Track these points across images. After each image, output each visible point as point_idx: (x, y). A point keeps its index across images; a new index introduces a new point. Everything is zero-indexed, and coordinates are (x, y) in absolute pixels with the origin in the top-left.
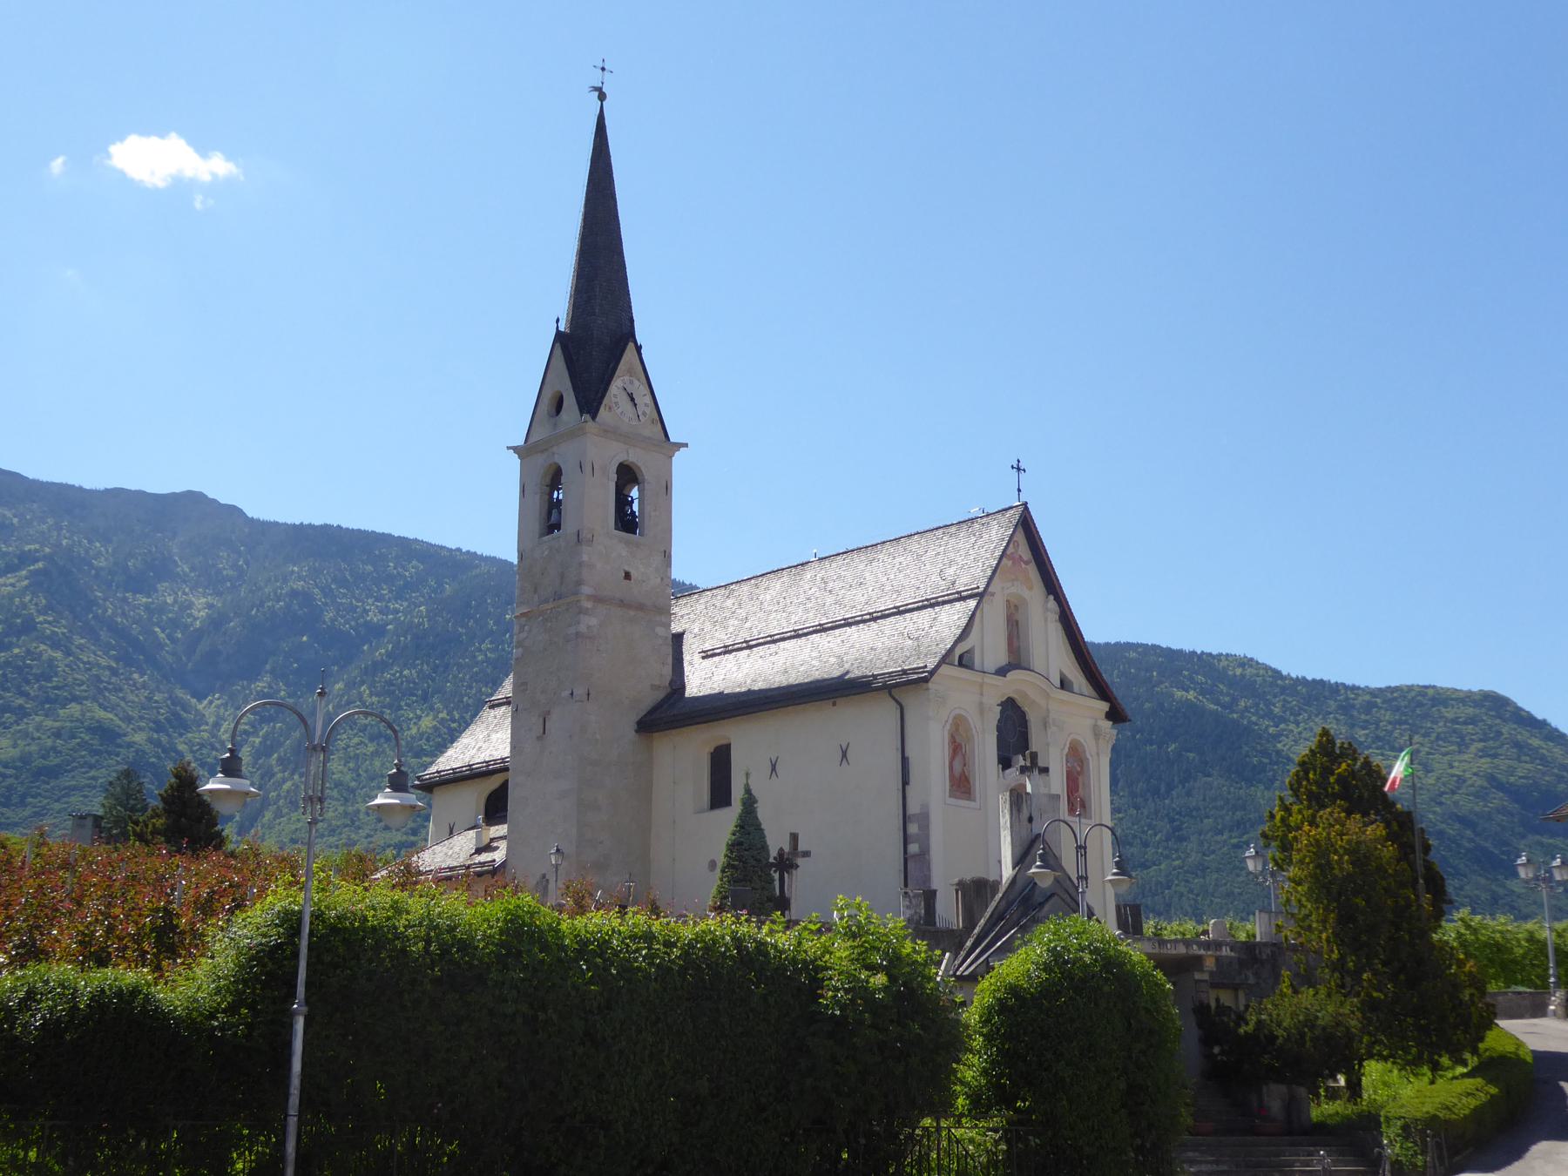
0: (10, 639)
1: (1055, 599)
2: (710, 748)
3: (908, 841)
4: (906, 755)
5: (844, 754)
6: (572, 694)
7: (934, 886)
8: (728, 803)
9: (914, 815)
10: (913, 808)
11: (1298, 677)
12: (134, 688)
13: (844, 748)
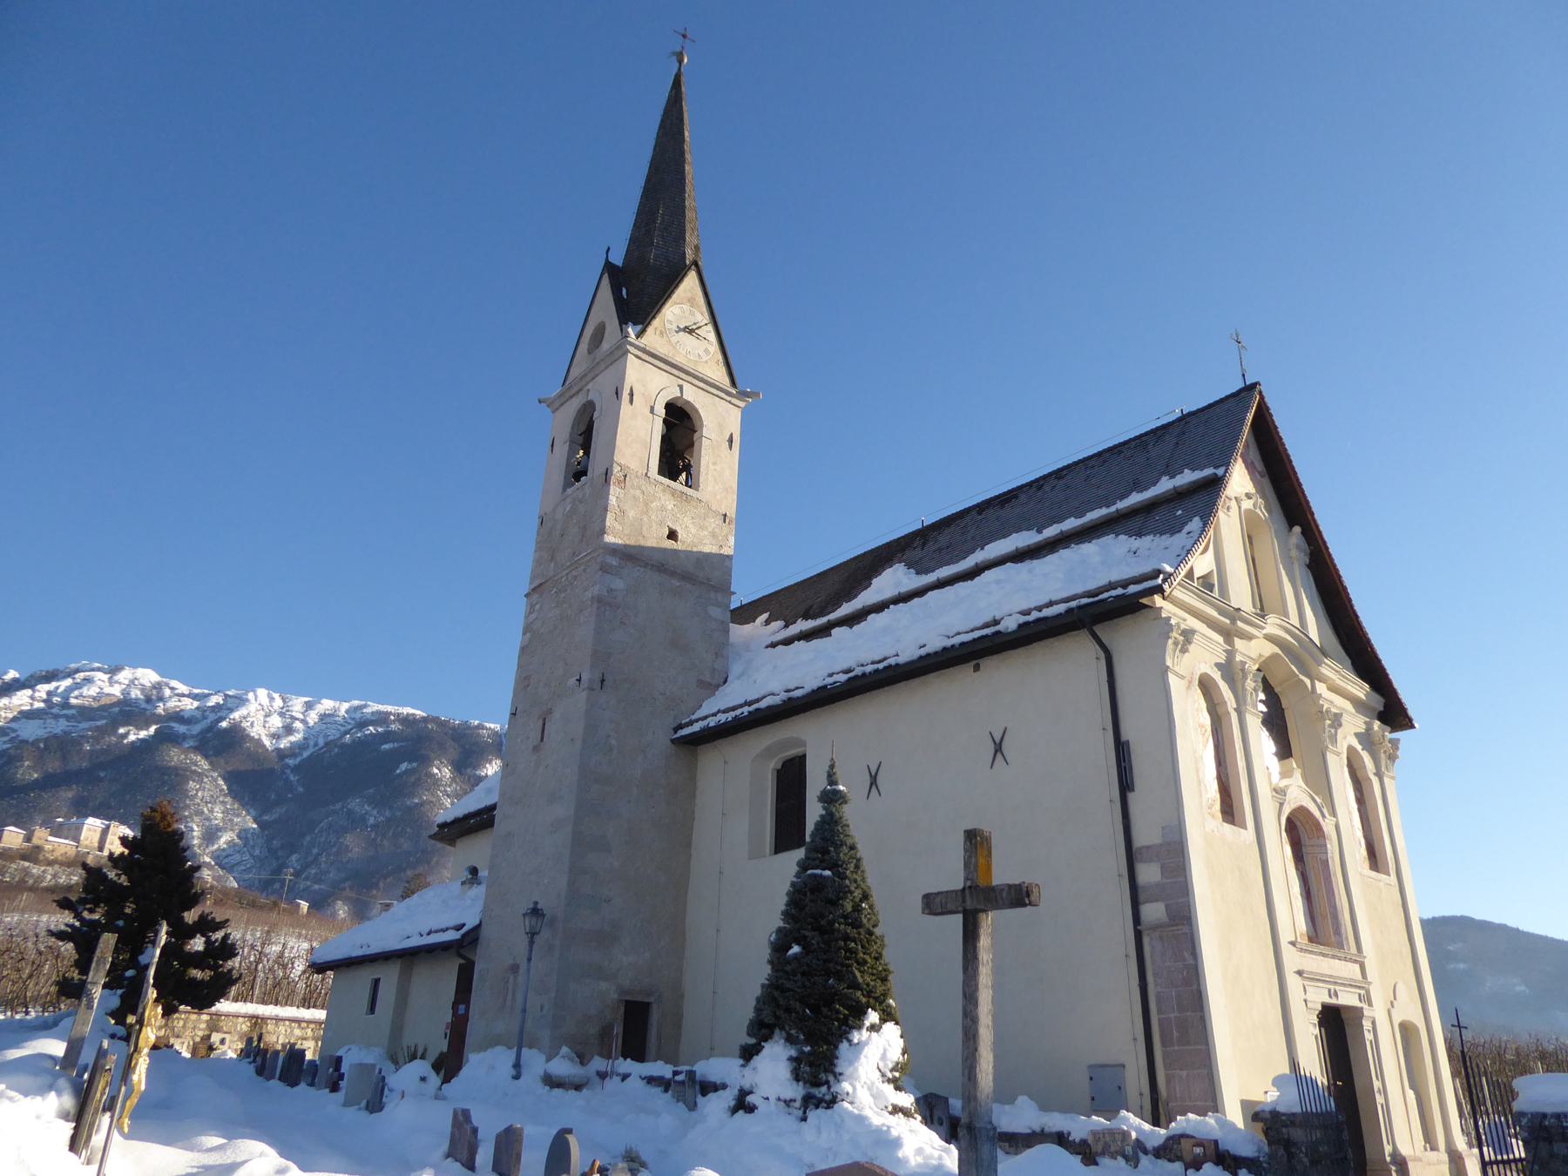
1: (1302, 533)
2: (774, 764)
3: (1142, 897)
4: (1124, 738)
5: (998, 748)
6: (579, 680)
9: (1148, 847)
10: (1144, 836)
11: (625, 1059)
13: (998, 741)
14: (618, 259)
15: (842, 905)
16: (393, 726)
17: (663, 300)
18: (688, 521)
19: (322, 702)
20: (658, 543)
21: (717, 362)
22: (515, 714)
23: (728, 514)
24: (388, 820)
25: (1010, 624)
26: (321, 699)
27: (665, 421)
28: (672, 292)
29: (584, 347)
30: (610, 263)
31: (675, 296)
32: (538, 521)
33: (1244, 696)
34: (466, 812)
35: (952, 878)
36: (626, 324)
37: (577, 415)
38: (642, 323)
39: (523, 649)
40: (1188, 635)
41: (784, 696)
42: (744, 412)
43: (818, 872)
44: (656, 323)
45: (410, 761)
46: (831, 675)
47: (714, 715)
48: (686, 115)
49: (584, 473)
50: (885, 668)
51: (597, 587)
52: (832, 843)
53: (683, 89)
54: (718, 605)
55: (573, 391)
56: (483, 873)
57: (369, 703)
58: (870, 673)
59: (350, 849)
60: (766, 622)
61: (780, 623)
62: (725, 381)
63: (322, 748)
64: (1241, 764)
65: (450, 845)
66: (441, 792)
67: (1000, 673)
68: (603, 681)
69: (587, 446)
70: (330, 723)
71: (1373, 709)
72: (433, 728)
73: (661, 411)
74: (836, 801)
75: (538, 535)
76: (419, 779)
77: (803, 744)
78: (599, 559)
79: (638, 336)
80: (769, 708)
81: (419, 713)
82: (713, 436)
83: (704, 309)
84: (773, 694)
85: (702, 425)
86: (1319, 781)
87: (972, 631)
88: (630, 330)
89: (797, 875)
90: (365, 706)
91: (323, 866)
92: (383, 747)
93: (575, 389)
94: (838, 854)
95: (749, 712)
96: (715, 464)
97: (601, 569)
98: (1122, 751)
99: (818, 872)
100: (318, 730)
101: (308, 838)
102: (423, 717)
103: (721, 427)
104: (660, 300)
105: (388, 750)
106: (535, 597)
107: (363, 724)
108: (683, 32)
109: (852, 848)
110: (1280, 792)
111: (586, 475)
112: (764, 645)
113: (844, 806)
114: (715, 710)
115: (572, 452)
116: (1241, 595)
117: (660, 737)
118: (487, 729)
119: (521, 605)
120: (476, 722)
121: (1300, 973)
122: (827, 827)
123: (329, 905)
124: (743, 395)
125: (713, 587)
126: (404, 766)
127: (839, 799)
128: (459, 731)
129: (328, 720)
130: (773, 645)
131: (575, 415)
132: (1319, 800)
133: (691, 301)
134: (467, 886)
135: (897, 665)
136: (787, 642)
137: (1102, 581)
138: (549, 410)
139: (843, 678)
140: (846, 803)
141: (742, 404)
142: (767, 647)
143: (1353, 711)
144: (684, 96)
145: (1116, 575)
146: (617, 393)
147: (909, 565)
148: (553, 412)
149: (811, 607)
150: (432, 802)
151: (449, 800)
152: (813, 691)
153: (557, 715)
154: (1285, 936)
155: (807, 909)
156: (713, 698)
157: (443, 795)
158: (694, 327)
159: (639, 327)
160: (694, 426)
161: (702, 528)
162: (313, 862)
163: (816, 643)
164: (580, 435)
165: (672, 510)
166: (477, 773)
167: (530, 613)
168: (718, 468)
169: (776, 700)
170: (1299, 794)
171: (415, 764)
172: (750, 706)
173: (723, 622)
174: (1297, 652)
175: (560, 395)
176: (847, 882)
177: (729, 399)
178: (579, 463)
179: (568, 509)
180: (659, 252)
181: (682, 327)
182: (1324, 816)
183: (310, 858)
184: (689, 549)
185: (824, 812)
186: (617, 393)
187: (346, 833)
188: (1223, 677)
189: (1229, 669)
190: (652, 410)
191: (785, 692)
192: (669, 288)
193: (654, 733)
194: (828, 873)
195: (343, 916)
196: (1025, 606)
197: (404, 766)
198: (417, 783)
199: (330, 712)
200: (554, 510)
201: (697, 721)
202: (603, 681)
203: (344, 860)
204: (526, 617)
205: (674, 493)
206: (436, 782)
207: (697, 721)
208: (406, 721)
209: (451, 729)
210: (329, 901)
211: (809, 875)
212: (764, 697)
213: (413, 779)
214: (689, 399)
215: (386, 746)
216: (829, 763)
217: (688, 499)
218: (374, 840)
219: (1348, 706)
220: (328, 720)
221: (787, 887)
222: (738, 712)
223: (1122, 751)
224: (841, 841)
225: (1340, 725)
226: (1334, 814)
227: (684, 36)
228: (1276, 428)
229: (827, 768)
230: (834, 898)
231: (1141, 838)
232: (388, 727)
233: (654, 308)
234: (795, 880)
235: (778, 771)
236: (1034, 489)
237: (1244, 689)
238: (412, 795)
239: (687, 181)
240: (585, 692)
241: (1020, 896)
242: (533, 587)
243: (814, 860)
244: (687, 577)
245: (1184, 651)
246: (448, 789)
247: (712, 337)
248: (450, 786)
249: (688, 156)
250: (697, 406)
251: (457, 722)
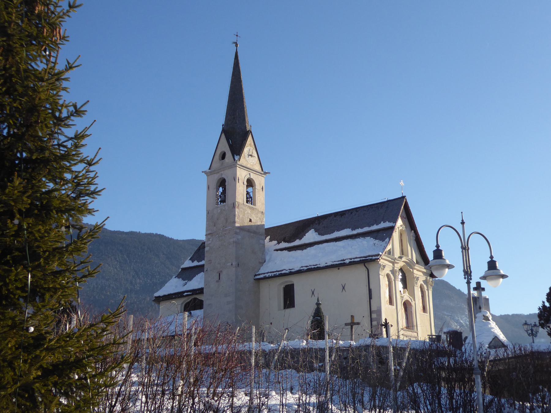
2: (283, 286)
4: (370, 288)
5: (344, 288)
6: (232, 264)
9: (374, 311)
10: (373, 309)
13: (343, 286)
18: (253, 215)
25: (347, 261)
33: (396, 277)
35: (349, 321)
40: (384, 266)
41: (289, 271)
46: (302, 267)
62: (260, 170)
64: (394, 292)
67: (343, 271)
71: (428, 274)
84: (285, 270)
86: (412, 294)
87: (338, 261)
96: (259, 197)
98: (370, 291)
103: (260, 184)
106: (209, 236)
109: (323, 313)
110: (402, 297)
116: (397, 254)
117: (251, 278)
121: (403, 335)
132: (411, 298)
133: (250, 145)
135: (320, 267)
136: (282, 250)
137: (367, 255)
143: (423, 275)
145: (370, 254)
147: (316, 231)
152: (297, 271)
154: (401, 327)
168: (260, 198)
169: (287, 272)
170: (407, 297)
174: (410, 264)
177: (261, 175)
182: (412, 301)
188: (391, 273)
189: (393, 272)
190: (244, 184)
194: (319, 318)
196: (350, 257)
202: (238, 265)
205: (250, 208)
217: (253, 209)
219: (421, 274)
222: (275, 273)
223: (370, 291)
225: (418, 280)
226: (415, 300)
227: (237, 36)
228: (409, 207)
231: (373, 309)
236: (350, 213)
237: (396, 275)
241: (358, 324)
244: (255, 232)
245: (383, 270)
247: (256, 155)
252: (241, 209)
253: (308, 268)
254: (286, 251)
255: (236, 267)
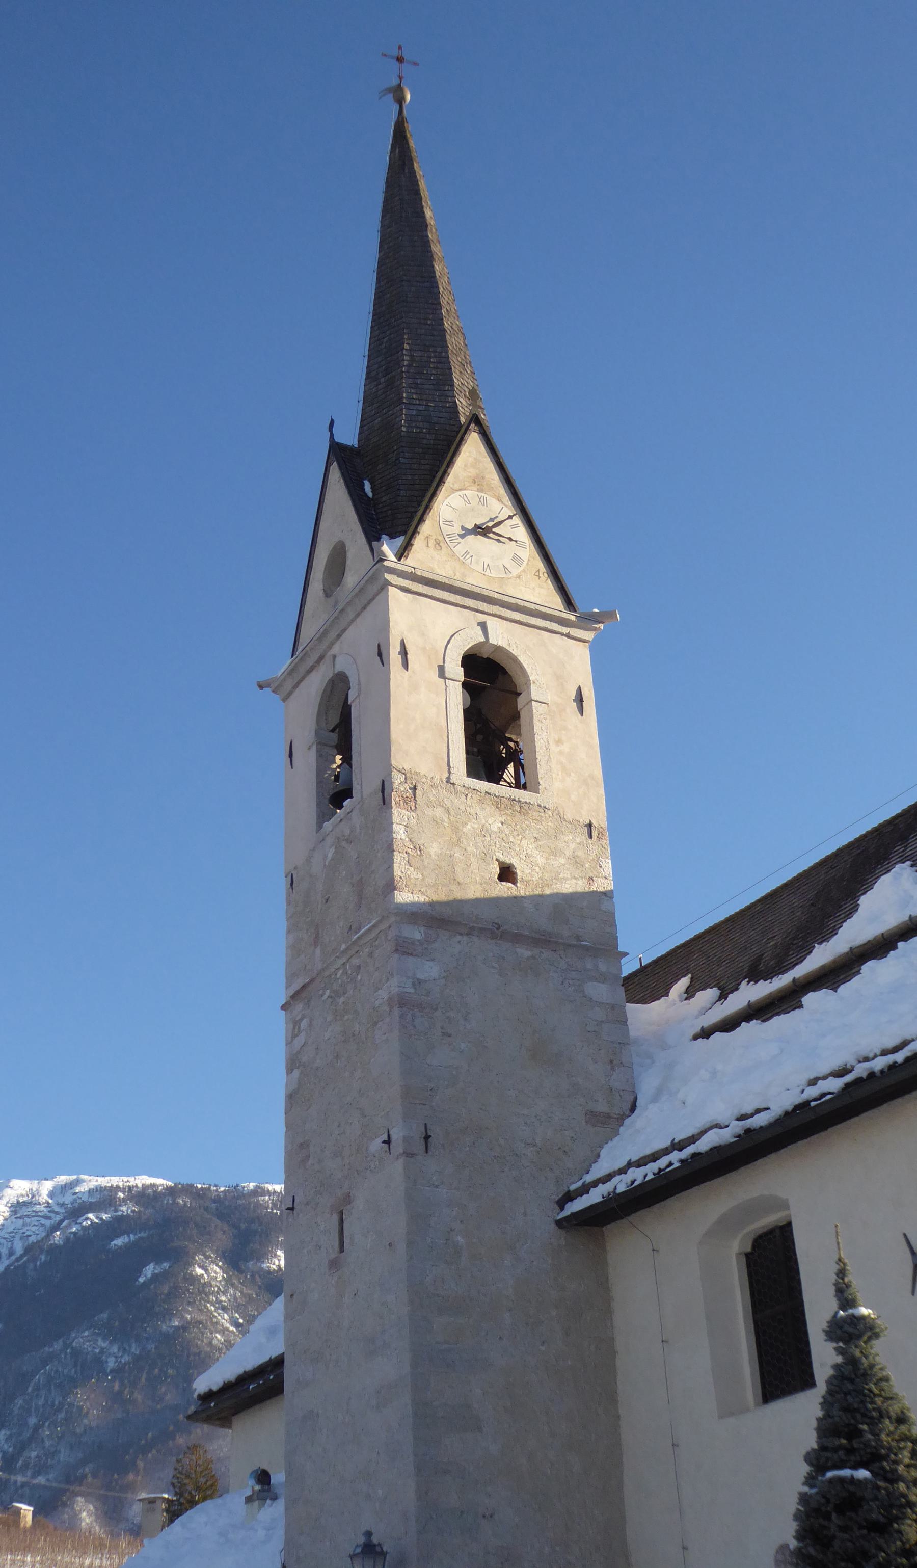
0: (136, 1237)
6: (388, 1142)
7: (285, 878)
8: (808, 1382)
12: (841, 1281)
14: (349, 436)
15: (900, 1532)
16: (124, 1209)
17: (432, 489)
18: (528, 845)
19: (11, 1184)
20: (484, 890)
21: (537, 574)
22: (292, 1209)
23: (594, 822)
24: (137, 1359)
26: (9, 1180)
27: (465, 685)
28: (445, 473)
29: (317, 585)
30: (338, 444)
31: (450, 480)
32: (283, 883)
34: (240, 1371)
36: (378, 539)
37: (322, 699)
38: (404, 533)
39: (292, 1098)
41: (737, 1127)
42: (596, 650)
43: (846, 1473)
44: (426, 528)
45: (158, 1262)
46: (813, 1082)
47: (623, 1171)
48: (422, 184)
49: (347, 793)
50: (908, 1060)
51: (395, 981)
52: (864, 1415)
53: (412, 143)
54: (603, 978)
55: (310, 662)
56: (278, 1478)
57: (82, 1177)
58: (882, 1071)
59: (85, 1410)
60: (686, 992)
61: (711, 993)
62: (551, 600)
63: (22, 1256)
65: (223, 1426)
66: (212, 1304)
68: (427, 1138)
69: (345, 747)
70: (27, 1216)
72: (185, 1204)
73: (457, 671)
74: (859, 1337)
75: (289, 903)
76: (176, 1287)
77: (785, 1205)
78: (392, 934)
79: (401, 554)
80: (716, 1150)
81: (161, 1182)
82: (548, 698)
83: (502, 491)
85: (528, 683)
88: (385, 548)
89: (810, 1480)
90: (78, 1182)
91: (47, 1443)
92: (115, 1242)
93: (314, 657)
94: (877, 1435)
95: (682, 1161)
96: (559, 742)
97: (396, 950)
99: (846, 1473)
100: (11, 1230)
101: (19, 1402)
102: (169, 1189)
104: (426, 491)
105: (120, 1248)
106: (299, 1007)
107: (77, 1211)
108: (396, 53)
109: (901, 1419)
111: (352, 797)
112: (691, 1037)
113: (874, 1342)
114: (621, 1163)
115: (324, 760)
118: (269, 1193)
119: (279, 1022)
120: (252, 1186)
122: (850, 1386)
123: (64, 1505)
124: (588, 620)
125: (587, 949)
126: (149, 1270)
127: (864, 1333)
128: (227, 1203)
129: (25, 1211)
130: (706, 1033)
131: (319, 699)
133: (478, 482)
134: (256, 1503)
136: (729, 1025)
138: (277, 698)
139: (835, 1085)
140: (877, 1336)
141: (589, 636)
142: (695, 1038)
144: (414, 154)
146: (380, 655)
148: (284, 700)
149: (760, 957)
150: (200, 1322)
151: (226, 1316)
152: (787, 1114)
153: (359, 1203)
155: (836, 1544)
156: (616, 1139)
157: (217, 1309)
158: (490, 524)
159: (400, 541)
160: (515, 686)
161: (554, 853)
162: (31, 1439)
163: (779, 1022)
164: (333, 731)
165: (501, 831)
166: (264, 1266)
167: (294, 1036)
168: (565, 747)
169: (724, 1137)
171: (166, 1265)
172: (680, 1150)
173: (613, 1007)
175: (291, 671)
176: (902, 1486)
177: (565, 630)
178: (337, 778)
179: (330, 855)
180: (414, 413)
181: (470, 526)
183: (27, 1434)
184: (538, 892)
185: (839, 1359)
186: (380, 655)
187: (76, 1387)
191: (738, 1119)
192: (439, 467)
193: (525, 1214)
194: (863, 1474)
195: (88, 1520)
197: (149, 1270)
198: (174, 1294)
199: (25, 1199)
200: (308, 860)
201: (595, 1184)
202: (427, 1138)
203: (78, 1431)
204: (289, 1043)
205: (498, 803)
206: (203, 1289)
207: (595, 1184)
208: (143, 1196)
209: (214, 1201)
210: (64, 1498)
211: (831, 1481)
212: (704, 1132)
213: (166, 1289)
214: (500, 643)
215: (119, 1242)
216: (836, 1268)
217: (523, 808)
218: (120, 1393)
220: (25, 1211)
221: (792, 1505)
222: (662, 1162)
224: (879, 1410)
227: (400, 60)
229: (833, 1278)
230: (882, 1519)
232: (116, 1211)
233: (419, 504)
234: (806, 1489)
235: (747, 1255)
238: (168, 1314)
239: (441, 290)
240: (401, 1161)
242: (292, 993)
243: (835, 1450)
246: (223, 1298)
247: (521, 533)
248: (224, 1293)
249: (436, 249)
250: (515, 651)
251: (222, 1189)
252: (429, 812)
253: (849, 1078)
254: (754, 1022)
255: (408, 1154)
